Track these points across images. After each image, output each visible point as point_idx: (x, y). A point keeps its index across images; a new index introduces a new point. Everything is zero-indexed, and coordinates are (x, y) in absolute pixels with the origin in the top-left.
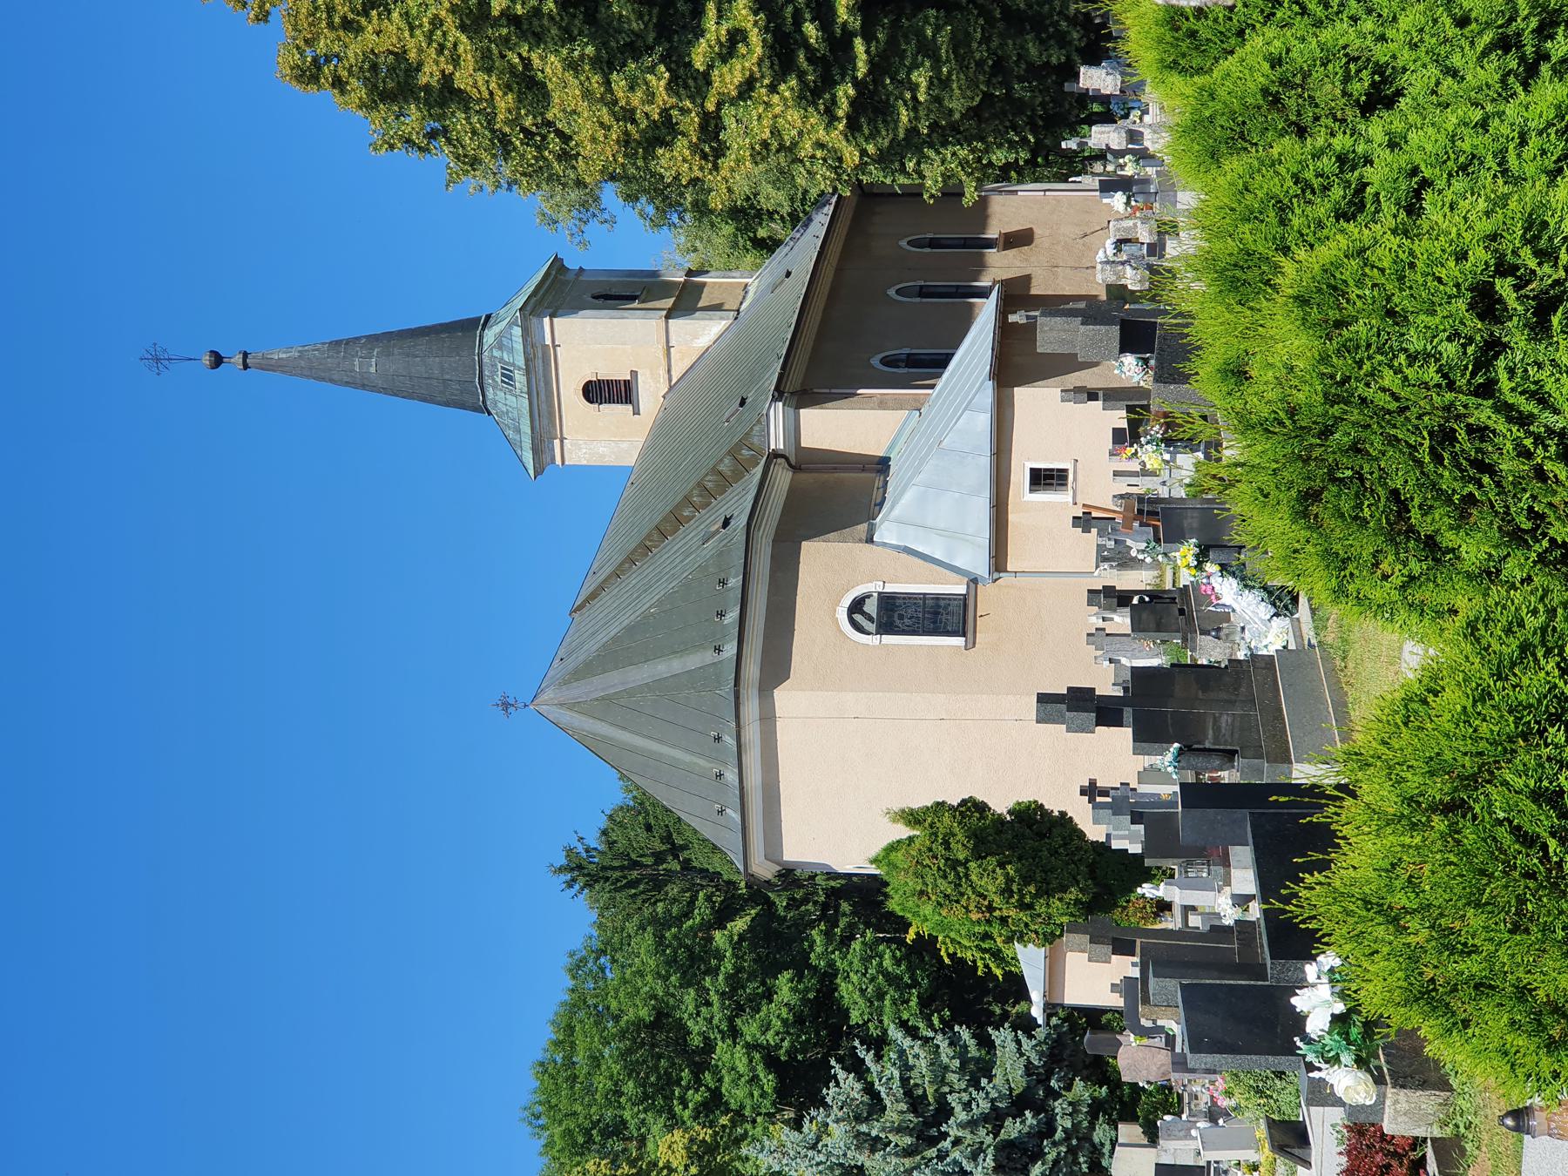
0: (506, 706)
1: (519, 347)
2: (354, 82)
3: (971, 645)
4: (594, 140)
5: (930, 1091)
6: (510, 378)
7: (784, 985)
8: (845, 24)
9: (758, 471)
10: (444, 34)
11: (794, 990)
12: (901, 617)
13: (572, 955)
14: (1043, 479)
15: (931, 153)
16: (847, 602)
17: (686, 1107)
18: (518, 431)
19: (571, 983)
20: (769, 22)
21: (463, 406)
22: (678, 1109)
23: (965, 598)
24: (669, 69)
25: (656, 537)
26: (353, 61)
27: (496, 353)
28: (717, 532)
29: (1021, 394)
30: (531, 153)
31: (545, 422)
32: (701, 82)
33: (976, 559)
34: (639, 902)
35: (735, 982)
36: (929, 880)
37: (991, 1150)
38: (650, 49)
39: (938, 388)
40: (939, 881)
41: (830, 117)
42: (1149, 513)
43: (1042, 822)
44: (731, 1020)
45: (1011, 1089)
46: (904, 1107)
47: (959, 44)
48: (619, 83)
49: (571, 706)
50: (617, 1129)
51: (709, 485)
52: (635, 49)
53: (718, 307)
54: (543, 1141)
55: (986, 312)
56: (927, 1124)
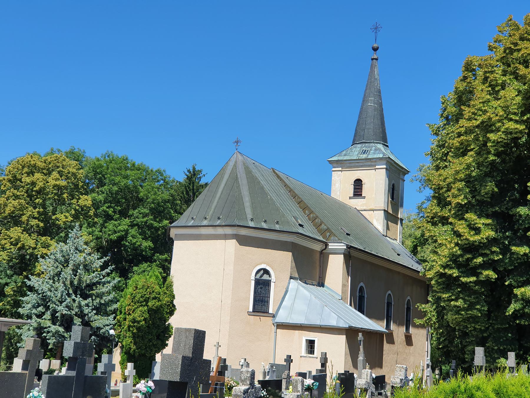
0: (237, 142)
1: (375, 156)
2: (465, 84)
3: (249, 314)
4: (440, 175)
5: (94, 292)
6: (364, 153)
7: (147, 244)
8: (482, 274)
9: (321, 238)
10: (480, 115)
11: (146, 247)
12: (261, 288)
13: (164, 171)
14: (311, 344)
15: (434, 307)
16: (268, 268)
17: (107, 208)
18: (345, 155)
19: (154, 170)
20: (483, 244)
21: (355, 136)
22: (106, 205)
23: (267, 312)
24: (465, 204)
25: (299, 200)
26: (473, 84)
27: (373, 148)
28: (298, 222)
29: (343, 338)
30: (439, 155)
31: (348, 165)
32: (460, 217)
33: (282, 317)
34: (181, 195)
35: (150, 227)
36: (141, 291)
37: (69, 313)
38: (473, 197)
39: (350, 307)
40: (140, 295)
41: (445, 267)
42: (216, 388)
43: (164, 336)
44: (137, 225)
45: (92, 321)
46: (88, 282)
47: (474, 319)
48: (461, 185)
49: (235, 165)
50: (101, 184)
51: (317, 220)
52: (474, 192)
53: (388, 228)
54: (100, 157)
55: (378, 326)
56: (82, 290)
